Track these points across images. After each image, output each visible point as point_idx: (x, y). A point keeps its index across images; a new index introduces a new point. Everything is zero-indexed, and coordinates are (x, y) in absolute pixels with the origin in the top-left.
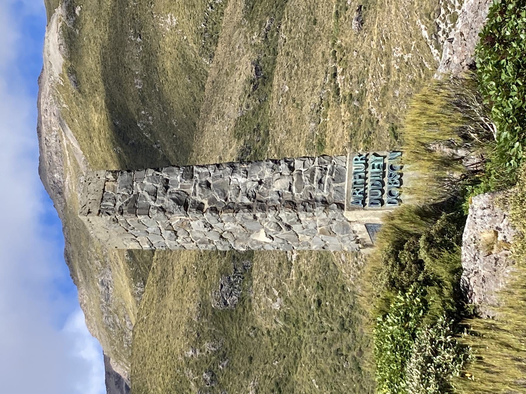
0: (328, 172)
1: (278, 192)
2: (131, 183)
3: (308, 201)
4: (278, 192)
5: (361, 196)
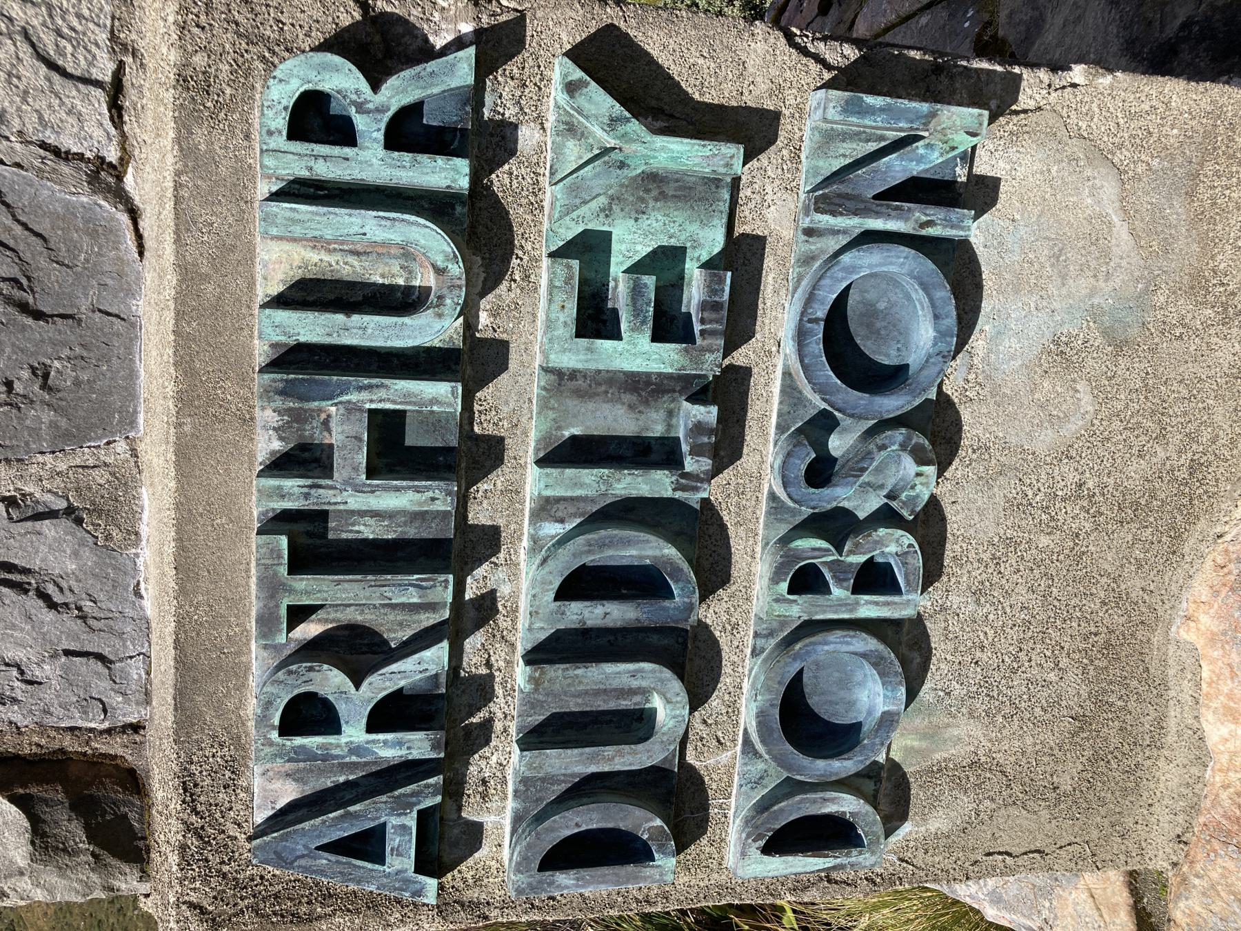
5: (419, 745)
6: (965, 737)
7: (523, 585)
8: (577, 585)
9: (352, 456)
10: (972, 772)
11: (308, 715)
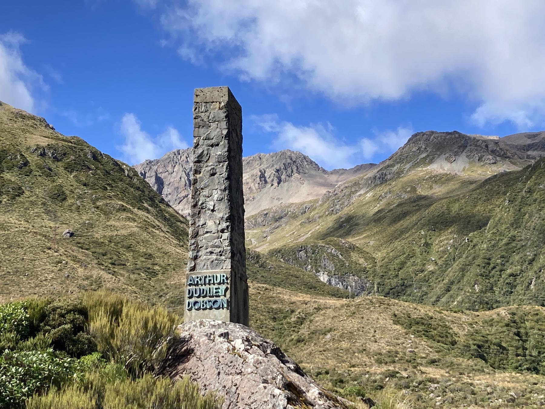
0: (219, 257)
2: (217, 120)
3: (197, 245)
5: (196, 282)
6: (193, 314)
7: (204, 287)
8: (203, 290)
9: (210, 278)
10: (191, 315)
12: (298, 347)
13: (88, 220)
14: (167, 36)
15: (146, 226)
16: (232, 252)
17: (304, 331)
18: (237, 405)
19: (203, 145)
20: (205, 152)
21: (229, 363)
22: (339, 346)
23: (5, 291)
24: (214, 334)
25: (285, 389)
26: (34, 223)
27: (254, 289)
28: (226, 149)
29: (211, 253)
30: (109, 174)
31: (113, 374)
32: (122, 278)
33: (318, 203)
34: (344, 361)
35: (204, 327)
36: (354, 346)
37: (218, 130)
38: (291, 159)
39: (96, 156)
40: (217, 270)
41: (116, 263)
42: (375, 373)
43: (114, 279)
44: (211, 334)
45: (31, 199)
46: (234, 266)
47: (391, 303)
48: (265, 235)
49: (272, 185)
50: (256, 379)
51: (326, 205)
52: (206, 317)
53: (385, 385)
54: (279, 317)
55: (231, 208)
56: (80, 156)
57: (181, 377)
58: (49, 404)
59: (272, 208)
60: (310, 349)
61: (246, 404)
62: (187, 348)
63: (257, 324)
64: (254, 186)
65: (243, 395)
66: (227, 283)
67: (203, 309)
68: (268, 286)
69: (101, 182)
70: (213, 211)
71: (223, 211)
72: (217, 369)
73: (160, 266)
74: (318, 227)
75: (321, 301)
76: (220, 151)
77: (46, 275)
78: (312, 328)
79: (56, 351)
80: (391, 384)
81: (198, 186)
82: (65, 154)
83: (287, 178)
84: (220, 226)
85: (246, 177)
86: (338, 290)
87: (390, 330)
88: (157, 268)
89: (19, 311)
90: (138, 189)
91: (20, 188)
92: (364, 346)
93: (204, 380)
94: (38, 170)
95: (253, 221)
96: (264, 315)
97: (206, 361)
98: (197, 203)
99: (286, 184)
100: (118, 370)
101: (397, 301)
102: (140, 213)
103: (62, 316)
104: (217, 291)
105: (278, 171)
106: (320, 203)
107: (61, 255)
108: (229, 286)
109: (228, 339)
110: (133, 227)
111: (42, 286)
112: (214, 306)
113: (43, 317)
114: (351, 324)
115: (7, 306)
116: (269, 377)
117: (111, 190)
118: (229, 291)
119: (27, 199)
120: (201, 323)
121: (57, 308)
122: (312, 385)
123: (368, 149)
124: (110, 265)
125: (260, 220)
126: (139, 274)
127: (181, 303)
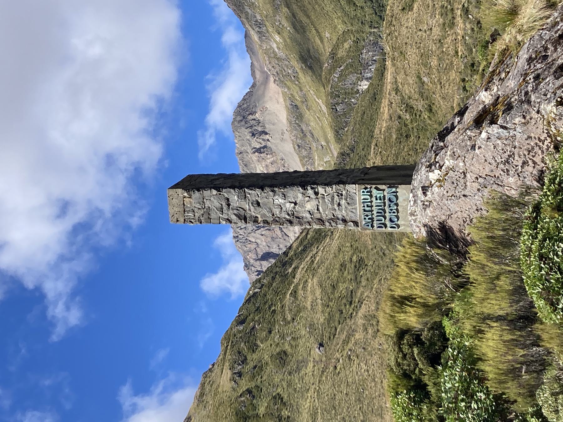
0: (343, 197)
1: (310, 211)
2: (202, 199)
3: (332, 219)
4: (310, 211)
5: (370, 221)
6: (403, 223)
7: (375, 212)
8: (378, 213)
9: (366, 206)
10: (404, 225)
11: (365, 219)
12: (436, 111)
13: (306, 329)
14: (122, 241)
15: (312, 270)
16: (338, 183)
17: (420, 105)
18: (498, 177)
19: (228, 215)
20: (235, 212)
21: (454, 186)
22: (436, 68)
23: (380, 412)
24: (424, 201)
25: (482, 126)
26: (310, 383)
27: (376, 158)
28: (232, 190)
29: (339, 205)
30: (258, 307)
31: (465, 305)
32: (366, 294)
33: (286, 92)
34: (452, 63)
35: (415, 211)
36: (435, 51)
37: (212, 198)
38: (241, 121)
39: (241, 321)
40: (357, 199)
41: (350, 300)
42: (464, 29)
43: (367, 302)
44: (423, 204)
45: (285, 386)
46: (353, 181)
47: (390, 14)
48: (320, 147)
49: (268, 140)
50: (471, 157)
51: (289, 83)
52: (405, 209)
53: (476, 19)
54: (406, 132)
55: (293, 185)
56: (241, 337)
57: (468, 235)
58: (497, 371)
59: (292, 140)
60: (439, 99)
61: (497, 167)
62: (439, 229)
63: (413, 154)
64: (270, 159)
65: (487, 171)
66: (371, 188)
67: (398, 212)
68: (373, 144)
69: (267, 316)
70: (295, 204)
71: (296, 193)
72: (460, 197)
73: (352, 256)
74: (312, 92)
75: (389, 87)
76: (234, 196)
77: (363, 370)
78: (417, 96)
79: (441, 363)
80: (474, 12)
81: (270, 219)
82: (239, 353)
83: (260, 124)
84: (312, 196)
85: (260, 169)
86: (377, 70)
87: (419, 14)
88: (354, 259)
89: (400, 400)
90: (273, 278)
91: (275, 397)
92: (435, 42)
93: (471, 211)
94: (255, 379)
95: (306, 159)
96: (404, 147)
97: (451, 210)
98: (287, 220)
99: (267, 126)
100: (461, 299)
101: (389, 8)
102: (298, 276)
103: (404, 356)
104: (378, 199)
105: (253, 135)
106: (286, 90)
107: (342, 356)
108: (374, 186)
109: (428, 187)
110: (313, 283)
111: (374, 375)
112: (394, 201)
113: (406, 375)
114: (412, 54)
115: (395, 413)
116: (468, 143)
117: (275, 306)
118: (379, 186)
119: (285, 390)
120: (412, 214)
121: (397, 361)
122: (477, 98)
123: (232, 36)
124: (353, 306)
125: (304, 153)
126: (361, 276)
127: (391, 234)
